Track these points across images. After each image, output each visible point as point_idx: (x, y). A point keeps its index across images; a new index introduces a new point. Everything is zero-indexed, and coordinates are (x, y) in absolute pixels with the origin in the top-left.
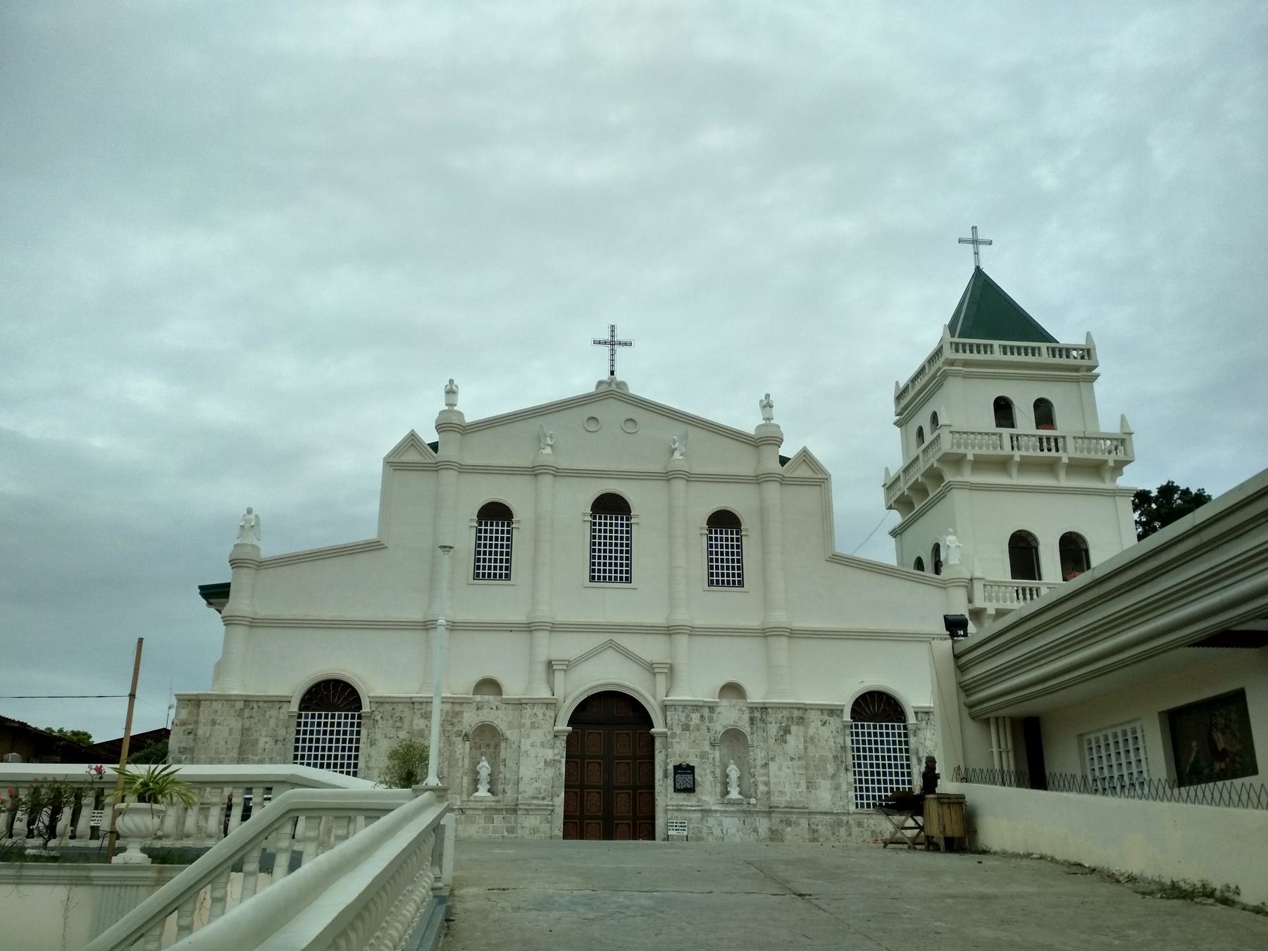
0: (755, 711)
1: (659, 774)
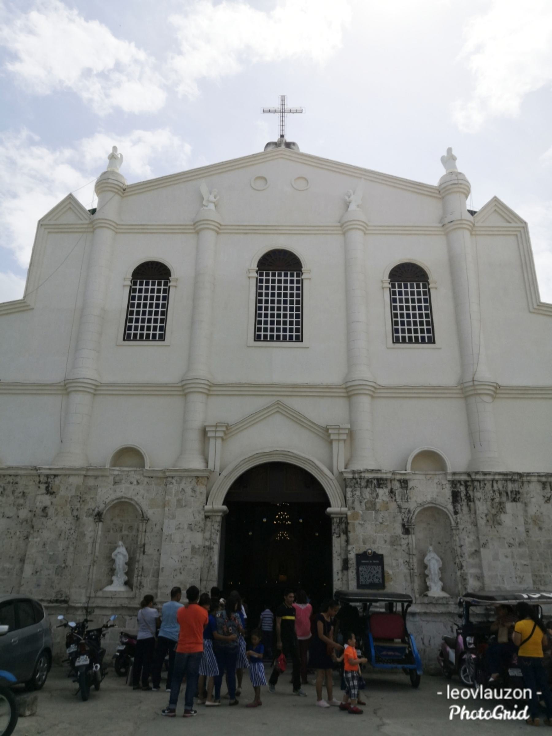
0: (458, 485)
1: (337, 565)
